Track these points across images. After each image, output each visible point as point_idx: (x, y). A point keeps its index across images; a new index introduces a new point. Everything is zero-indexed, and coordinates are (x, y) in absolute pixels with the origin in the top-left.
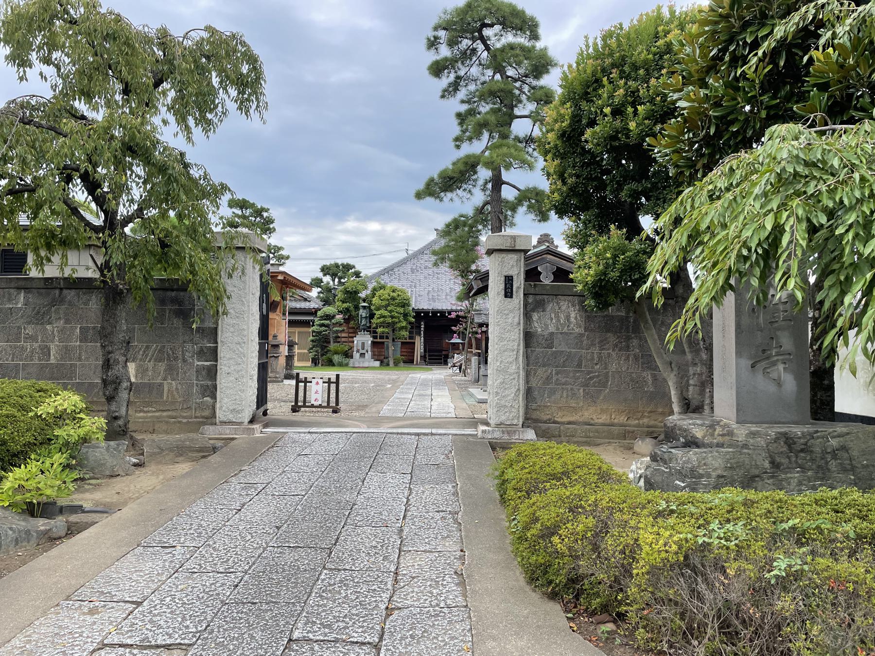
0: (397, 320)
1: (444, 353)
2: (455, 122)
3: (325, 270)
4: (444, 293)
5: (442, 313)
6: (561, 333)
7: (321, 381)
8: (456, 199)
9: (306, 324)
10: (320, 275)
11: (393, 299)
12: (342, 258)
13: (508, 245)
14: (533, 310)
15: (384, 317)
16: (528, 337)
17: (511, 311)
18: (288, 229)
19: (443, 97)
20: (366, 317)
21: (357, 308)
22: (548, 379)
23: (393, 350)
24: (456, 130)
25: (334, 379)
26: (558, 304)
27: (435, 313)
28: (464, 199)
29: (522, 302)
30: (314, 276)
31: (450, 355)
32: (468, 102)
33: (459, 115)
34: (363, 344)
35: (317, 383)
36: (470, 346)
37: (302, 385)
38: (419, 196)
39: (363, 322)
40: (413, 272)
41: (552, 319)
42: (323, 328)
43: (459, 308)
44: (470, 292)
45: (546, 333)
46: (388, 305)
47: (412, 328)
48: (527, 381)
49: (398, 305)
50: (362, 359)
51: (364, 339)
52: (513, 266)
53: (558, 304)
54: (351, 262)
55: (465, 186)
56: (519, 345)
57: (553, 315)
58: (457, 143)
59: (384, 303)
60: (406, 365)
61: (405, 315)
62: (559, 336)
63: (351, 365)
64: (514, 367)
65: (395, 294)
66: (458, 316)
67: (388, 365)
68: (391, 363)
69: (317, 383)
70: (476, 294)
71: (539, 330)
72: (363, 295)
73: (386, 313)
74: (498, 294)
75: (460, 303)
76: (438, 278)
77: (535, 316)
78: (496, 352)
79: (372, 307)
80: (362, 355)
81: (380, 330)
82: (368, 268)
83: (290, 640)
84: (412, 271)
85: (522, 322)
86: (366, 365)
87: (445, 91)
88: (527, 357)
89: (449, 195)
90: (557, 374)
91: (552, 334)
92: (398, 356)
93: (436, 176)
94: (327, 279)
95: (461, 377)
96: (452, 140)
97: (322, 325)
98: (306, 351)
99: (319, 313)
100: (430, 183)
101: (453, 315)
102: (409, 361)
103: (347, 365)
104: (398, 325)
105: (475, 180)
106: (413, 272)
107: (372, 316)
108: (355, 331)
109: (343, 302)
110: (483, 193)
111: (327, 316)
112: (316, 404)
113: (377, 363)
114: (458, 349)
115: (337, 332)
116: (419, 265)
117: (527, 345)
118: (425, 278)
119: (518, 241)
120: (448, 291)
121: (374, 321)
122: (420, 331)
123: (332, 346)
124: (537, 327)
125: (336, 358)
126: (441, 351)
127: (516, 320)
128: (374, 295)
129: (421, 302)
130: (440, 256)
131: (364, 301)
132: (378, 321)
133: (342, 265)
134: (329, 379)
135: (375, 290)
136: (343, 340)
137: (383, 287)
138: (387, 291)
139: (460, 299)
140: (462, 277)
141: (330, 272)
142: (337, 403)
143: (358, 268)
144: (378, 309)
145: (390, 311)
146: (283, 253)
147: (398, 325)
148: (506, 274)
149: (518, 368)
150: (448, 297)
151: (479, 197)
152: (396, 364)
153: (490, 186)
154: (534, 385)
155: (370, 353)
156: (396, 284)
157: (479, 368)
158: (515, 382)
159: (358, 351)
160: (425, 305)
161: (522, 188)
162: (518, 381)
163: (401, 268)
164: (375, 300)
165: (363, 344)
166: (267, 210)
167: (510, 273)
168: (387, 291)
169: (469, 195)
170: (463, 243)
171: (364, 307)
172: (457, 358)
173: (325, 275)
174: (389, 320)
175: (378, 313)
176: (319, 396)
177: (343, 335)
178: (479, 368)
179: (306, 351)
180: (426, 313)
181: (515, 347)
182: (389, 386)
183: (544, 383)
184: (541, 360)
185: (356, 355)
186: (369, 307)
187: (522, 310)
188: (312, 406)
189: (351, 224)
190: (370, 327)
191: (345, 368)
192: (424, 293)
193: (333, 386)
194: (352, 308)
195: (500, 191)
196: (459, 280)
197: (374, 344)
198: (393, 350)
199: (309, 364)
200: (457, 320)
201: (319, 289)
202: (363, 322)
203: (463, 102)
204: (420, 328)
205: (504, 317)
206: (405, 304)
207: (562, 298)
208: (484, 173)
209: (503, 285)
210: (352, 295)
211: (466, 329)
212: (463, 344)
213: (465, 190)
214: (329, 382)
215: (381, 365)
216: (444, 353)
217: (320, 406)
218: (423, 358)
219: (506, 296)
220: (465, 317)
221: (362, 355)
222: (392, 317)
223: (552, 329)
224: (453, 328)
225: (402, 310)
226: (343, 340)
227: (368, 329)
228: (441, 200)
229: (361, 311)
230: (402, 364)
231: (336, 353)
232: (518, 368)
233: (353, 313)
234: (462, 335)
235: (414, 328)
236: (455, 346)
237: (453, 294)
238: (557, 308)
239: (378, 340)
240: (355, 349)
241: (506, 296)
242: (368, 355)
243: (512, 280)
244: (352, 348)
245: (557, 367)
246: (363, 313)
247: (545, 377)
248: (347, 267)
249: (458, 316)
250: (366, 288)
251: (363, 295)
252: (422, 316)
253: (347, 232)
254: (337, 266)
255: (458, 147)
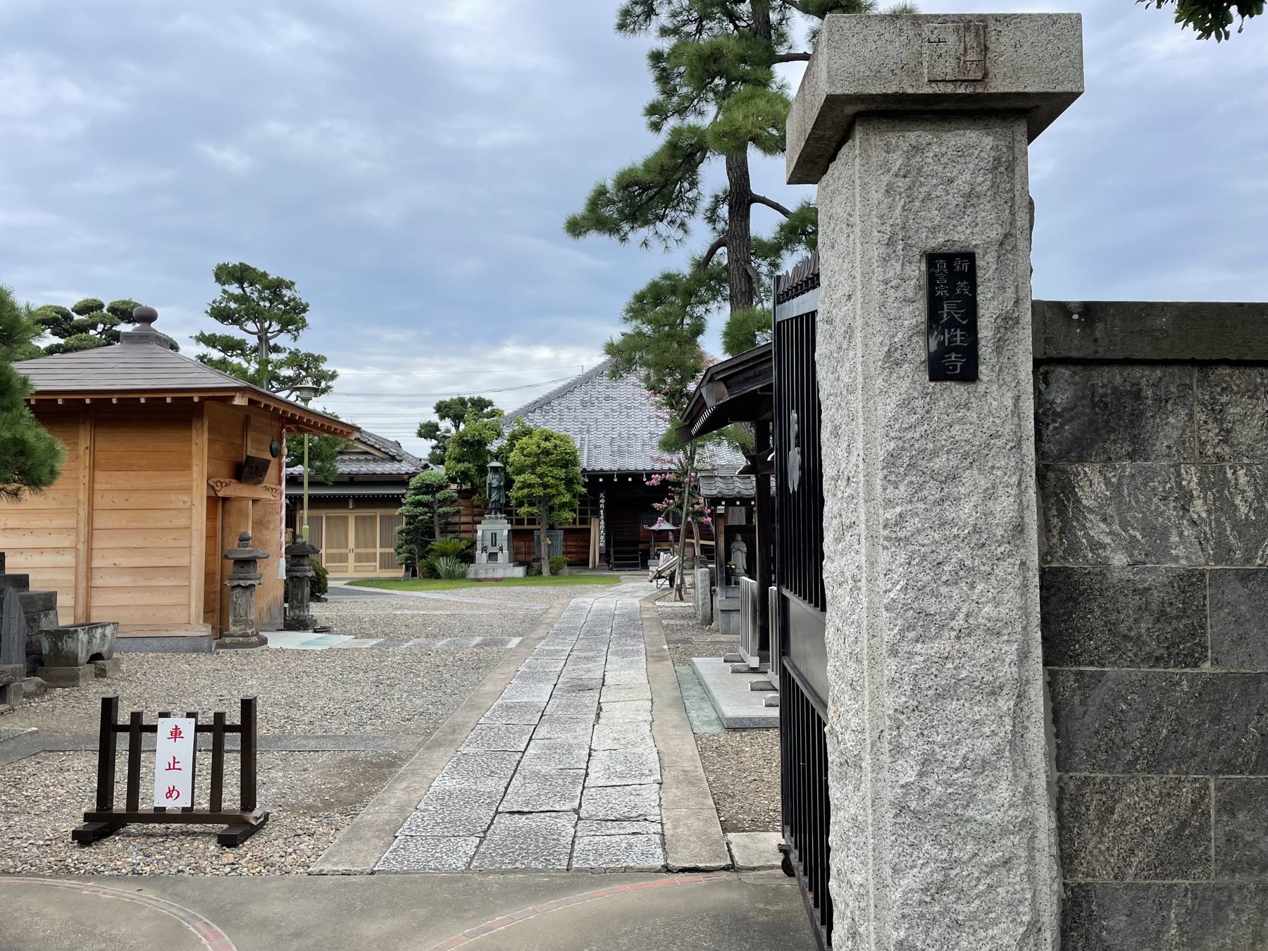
0: (554, 491)
1: (641, 546)
2: (648, 77)
3: (443, 409)
4: (640, 443)
5: (637, 475)
6: (1244, 577)
7: (188, 726)
8: (654, 242)
9: (396, 501)
10: (435, 418)
11: (547, 453)
12: (467, 391)
13: (947, 68)
14: (1081, 450)
15: (530, 486)
16: (1064, 599)
17: (973, 459)
18: (420, 360)
19: (622, 27)
20: (499, 488)
21: (483, 471)
22: (1185, 835)
23: (548, 545)
24: (653, 93)
25: (234, 718)
26: (1217, 412)
27: (623, 475)
28: (671, 243)
29: (1028, 406)
30: (425, 420)
31: (654, 550)
32: (675, 31)
33: (656, 57)
34: (494, 536)
35: (176, 733)
36: (689, 534)
37: (122, 742)
38: (576, 228)
39: (494, 497)
40: (584, 407)
41: (1185, 501)
42: (420, 510)
43: (666, 467)
44: (692, 425)
45: (1156, 577)
46: (538, 464)
47: (583, 503)
48: (1066, 860)
49: (555, 464)
50: (492, 565)
51: (494, 528)
52: (970, 197)
53: (1217, 412)
54: (487, 396)
55: (671, 214)
56: (1023, 656)
57: (1191, 478)
58: (655, 118)
59: (529, 461)
60: (575, 571)
61: (569, 482)
62: (1235, 592)
63: (471, 576)
64: (1003, 792)
65: (548, 445)
66: (664, 482)
67: (540, 573)
68: (546, 570)
69: (176, 733)
70: (705, 430)
71: (1119, 559)
72: (494, 447)
73: (533, 479)
74: (892, 359)
75: (666, 456)
76: (628, 416)
77: (1092, 484)
78: (890, 701)
79: (509, 469)
80: (493, 557)
81: (523, 510)
82: (507, 403)
83: (497, 812)
84: (584, 404)
85: (1032, 520)
86: (499, 574)
87: (626, 13)
88: (1058, 716)
89: (644, 232)
90: (1228, 807)
91: (1190, 581)
92: (559, 556)
93: (610, 185)
94: (446, 424)
95: (671, 604)
96: (643, 111)
97: (418, 504)
98: (392, 550)
99: (414, 482)
100: (599, 198)
101: (655, 481)
102: (580, 561)
103: (463, 576)
104: (556, 501)
105: (693, 202)
106: (584, 407)
107: (509, 484)
108: (480, 513)
109: (459, 461)
110: (710, 226)
111: (427, 486)
112: (172, 805)
113: (520, 571)
114: (666, 540)
115: (446, 515)
116: (595, 394)
117: (1059, 645)
118: (606, 416)
119: (1002, 46)
120: (647, 436)
121: (513, 493)
122: (599, 509)
123: (439, 542)
124: (1109, 545)
125: (442, 564)
126: (637, 543)
127: (1004, 507)
128: (512, 446)
129: (599, 456)
130: (623, 357)
131: (497, 457)
132: (520, 493)
133: (471, 400)
134: (219, 717)
135: (514, 437)
136: (463, 527)
137: (528, 433)
138: (535, 439)
139: (668, 445)
140: (672, 406)
141: (451, 412)
142: (248, 798)
143: (498, 405)
144: (520, 471)
145: (541, 476)
146: (324, 367)
147: (556, 501)
148: (935, 242)
149: (1028, 791)
150: (647, 448)
151: (699, 237)
152: (555, 572)
153: (724, 210)
154: (1105, 876)
155: (506, 551)
156: (554, 427)
157: (712, 593)
158: (1015, 877)
159: (484, 549)
160: (605, 463)
161: (792, 207)
162: (1031, 877)
163: (565, 402)
164: (514, 456)
165: (494, 536)
166: (289, 286)
167: (961, 236)
168: (535, 439)
169: (680, 234)
170: (672, 326)
171: (495, 469)
172: (665, 561)
173: (442, 418)
174: (539, 492)
175: (519, 479)
176: (182, 780)
177: (464, 519)
178: (712, 593)
179: (392, 550)
180: (608, 476)
181: (1007, 671)
182: (515, 641)
183: (1160, 865)
184: (1135, 729)
185: (481, 557)
186: (504, 469)
187: (1029, 448)
188: (160, 815)
189: (510, 351)
190: (508, 503)
191: (459, 582)
192: (604, 443)
193: (233, 741)
194: (473, 472)
195: (746, 216)
196: (666, 413)
197: (514, 534)
198: (548, 545)
199: (400, 573)
200: (663, 490)
201: (434, 442)
202: (494, 497)
203: (664, 32)
204: (599, 504)
205: (932, 491)
206: (568, 461)
207: (1238, 378)
208: (713, 174)
209: (921, 305)
210: (473, 448)
211: (680, 507)
212: (676, 533)
213: (672, 222)
214: (218, 727)
215: (527, 573)
216: (641, 546)
217: (187, 815)
218: (605, 557)
219: (939, 369)
220: (679, 484)
221: (493, 557)
222: (545, 486)
223: (1185, 552)
224: (656, 505)
225: (562, 473)
226: (463, 527)
227: (506, 510)
228: (623, 239)
229: (490, 476)
230: (566, 570)
231: (444, 554)
232: (1028, 791)
233: (477, 481)
234: (674, 518)
235: (587, 506)
236: (662, 535)
237: (655, 442)
238: (1212, 433)
239: (526, 527)
240: (479, 546)
241: (939, 369)
242: (503, 556)
243: (971, 277)
244: (473, 544)
245: (1229, 766)
246: (492, 479)
247: (1162, 829)
248: (480, 404)
249: (664, 482)
250: (499, 435)
251: (494, 447)
252: (600, 482)
253: (503, 361)
254: (462, 402)
255: (656, 127)
